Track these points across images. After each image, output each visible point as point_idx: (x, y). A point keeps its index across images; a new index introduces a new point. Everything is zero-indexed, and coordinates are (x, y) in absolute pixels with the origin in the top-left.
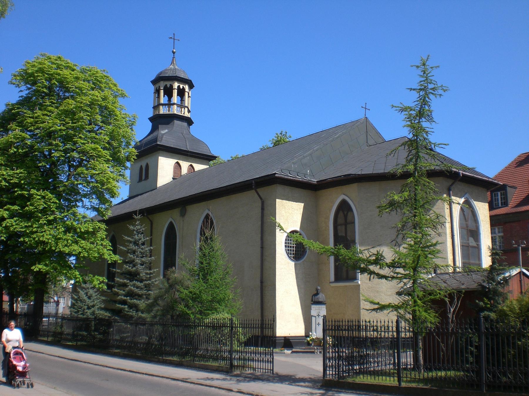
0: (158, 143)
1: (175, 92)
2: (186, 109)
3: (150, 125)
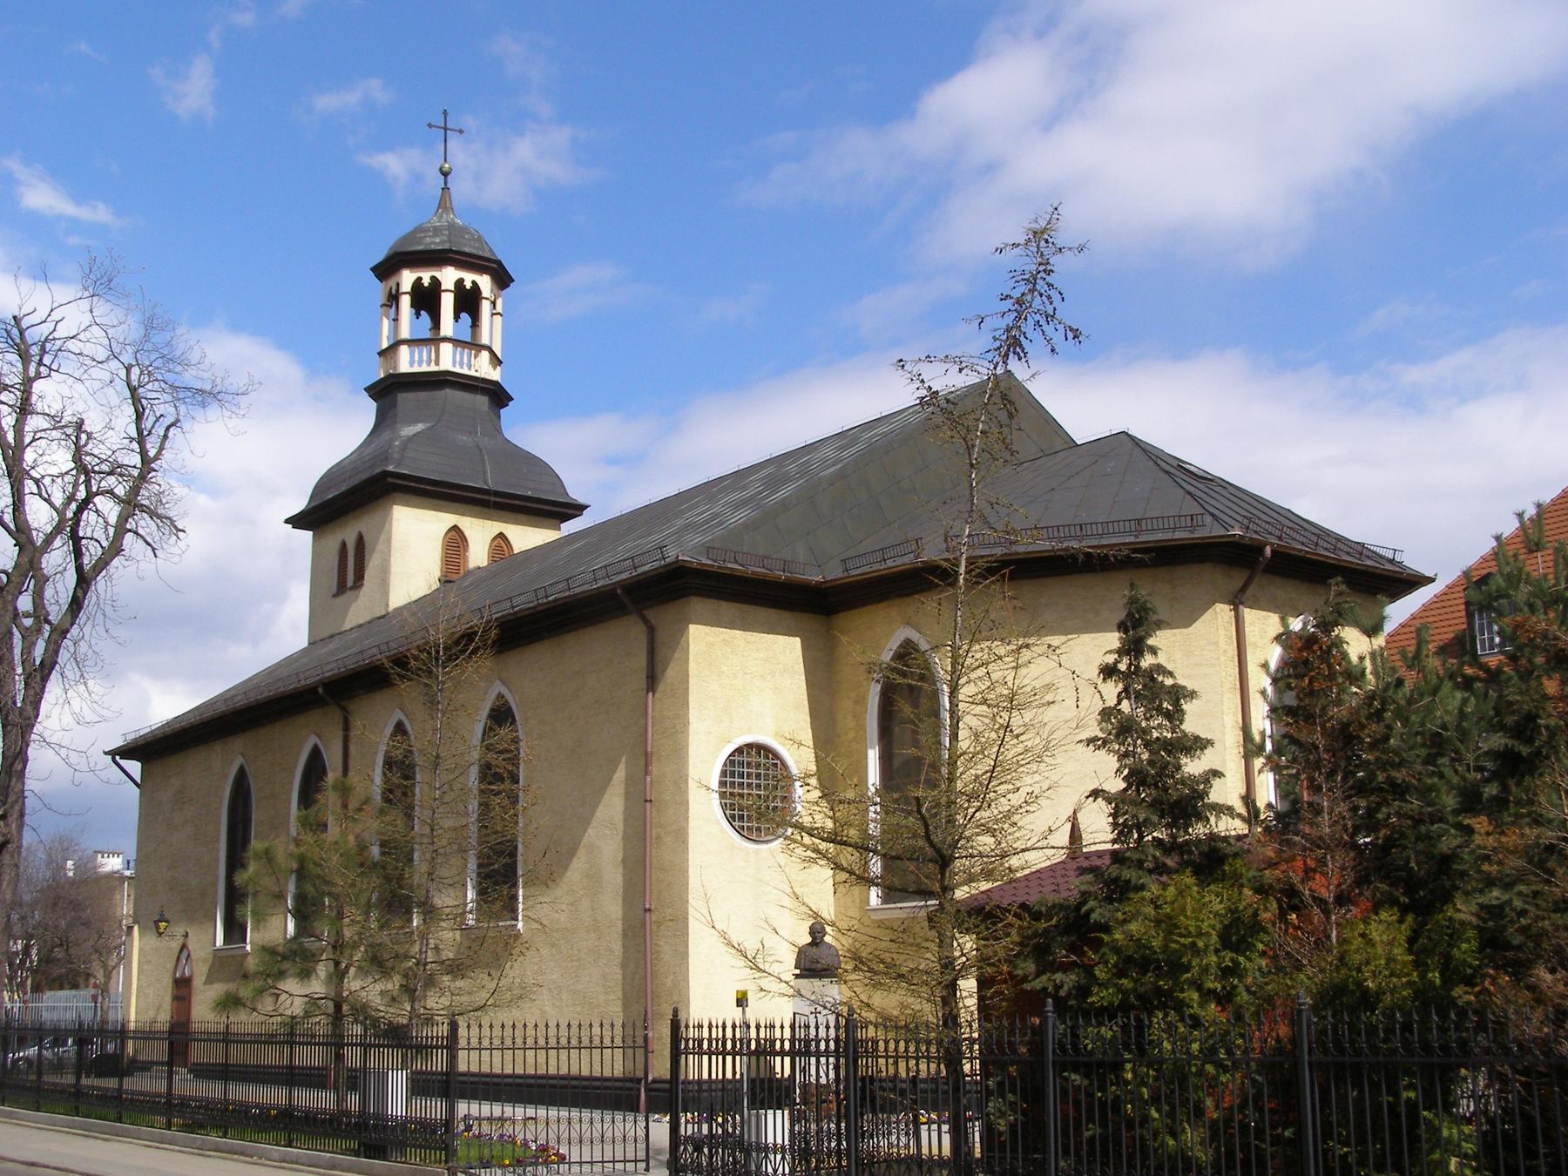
0: (391, 468)
1: (447, 302)
2: (485, 355)
3: (371, 406)
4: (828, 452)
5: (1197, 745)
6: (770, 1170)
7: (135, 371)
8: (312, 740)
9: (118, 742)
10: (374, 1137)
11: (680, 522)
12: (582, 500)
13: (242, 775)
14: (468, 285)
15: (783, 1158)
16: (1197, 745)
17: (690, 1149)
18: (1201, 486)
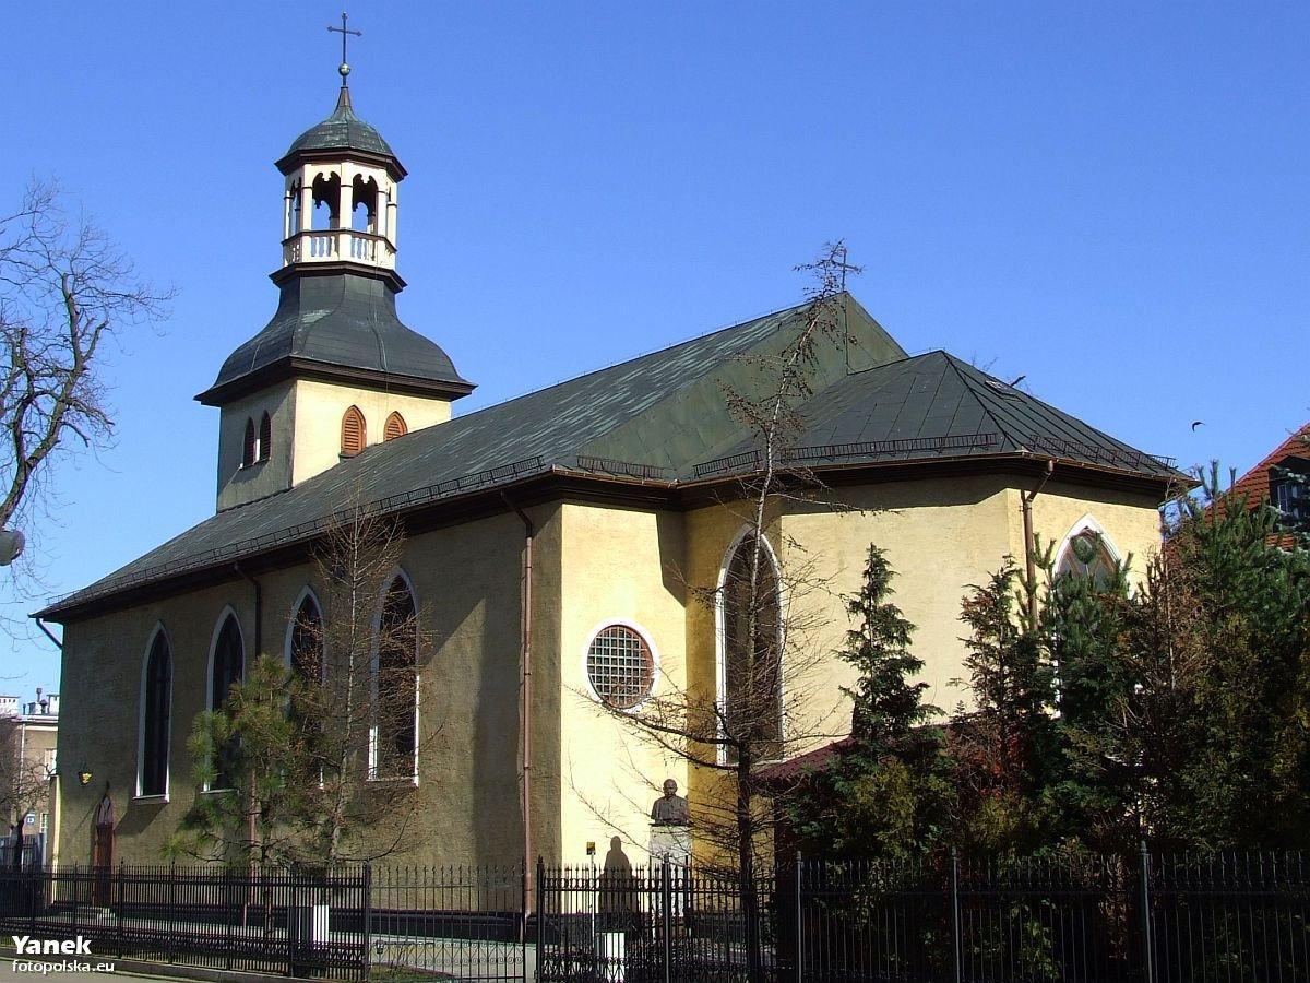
0: (294, 354)
1: (346, 196)
2: (381, 245)
4: (686, 360)
5: (913, 664)
6: (609, 978)
7: (70, 279)
8: (227, 610)
9: (42, 606)
10: (305, 958)
11: (558, 421)
12: (471, 381)
13: (160, 638)
14: (365, 180)
15: (619, 968)
16: (913, 664)
17: (551, 962)
18: (999, 401)
